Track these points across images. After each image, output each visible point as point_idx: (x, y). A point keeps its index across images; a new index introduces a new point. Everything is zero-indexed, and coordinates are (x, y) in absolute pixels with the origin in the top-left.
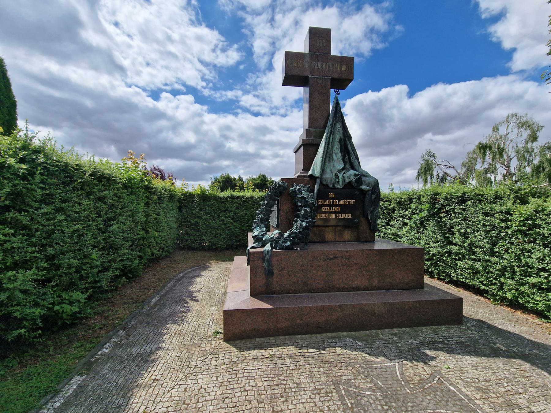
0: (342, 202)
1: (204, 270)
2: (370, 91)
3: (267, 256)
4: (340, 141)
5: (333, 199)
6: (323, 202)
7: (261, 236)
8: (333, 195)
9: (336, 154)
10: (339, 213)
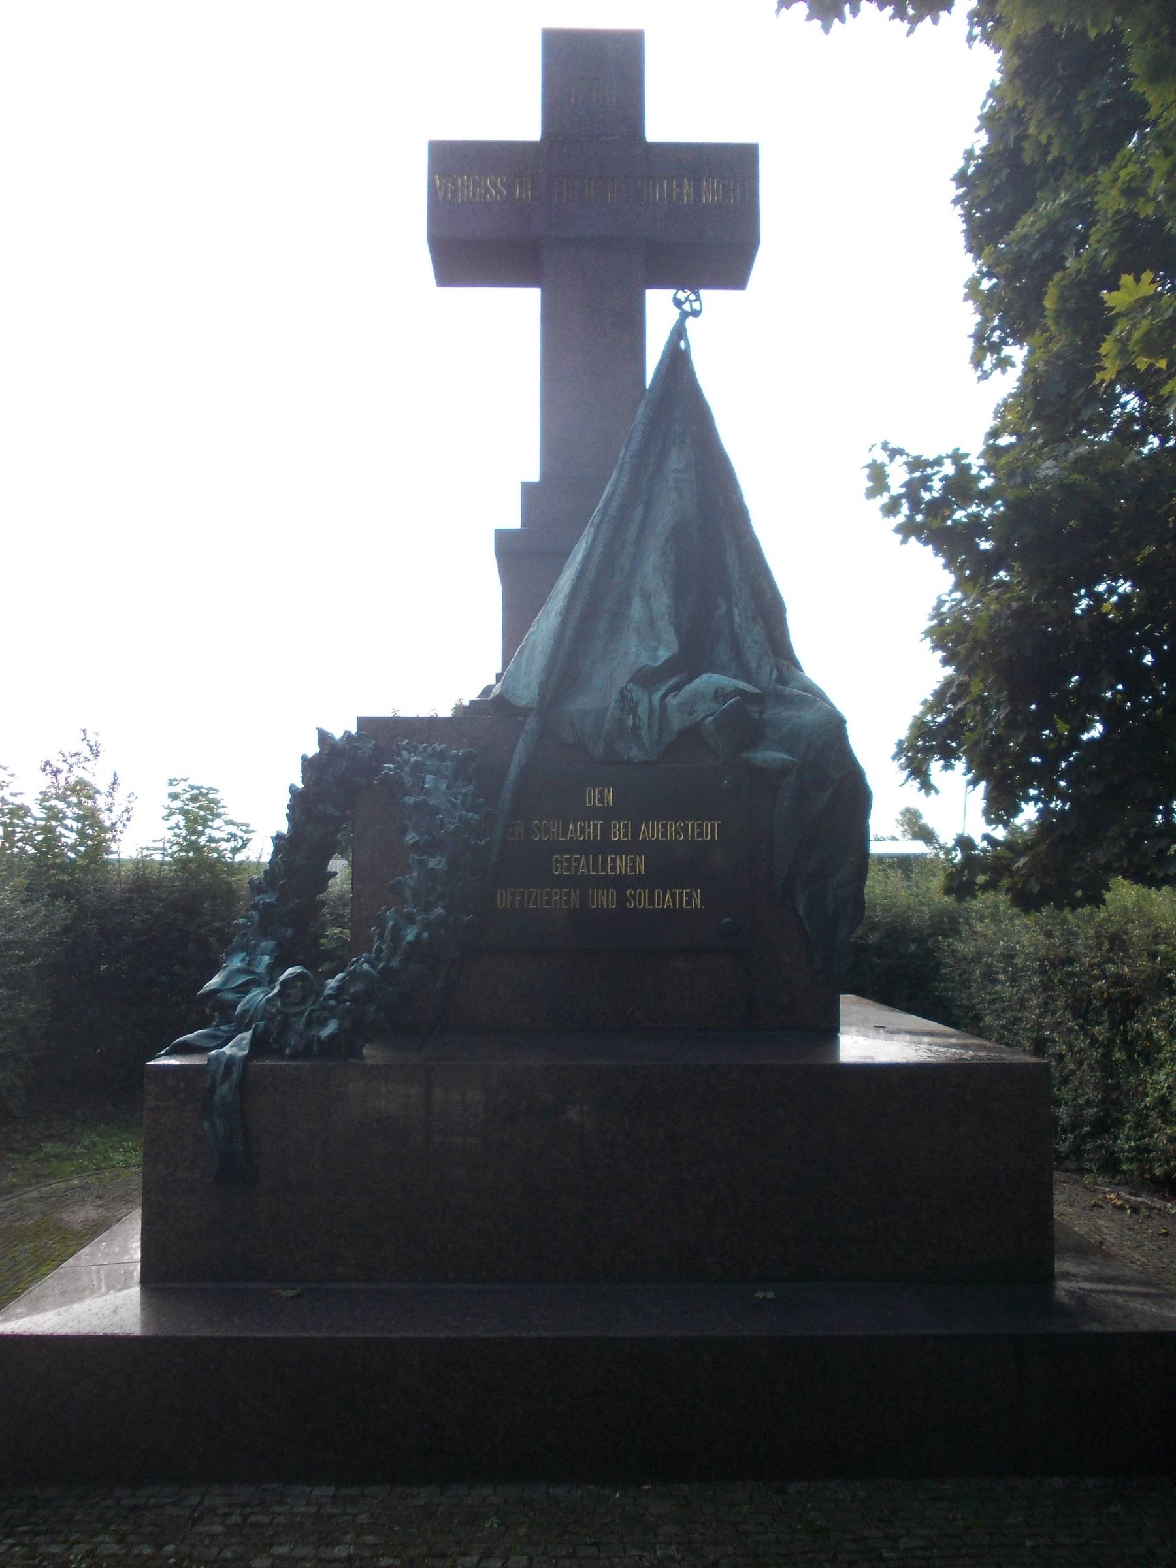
0: (651, 831)
1: (988, 797)
2: (354, 730)
3: (224, 1089)
4: (679, 531)
5: (607, 815)
6: (555, 827)
7: (230, 996)
8: (609, 796)
9: (647, 599)
10: (638, 882)
